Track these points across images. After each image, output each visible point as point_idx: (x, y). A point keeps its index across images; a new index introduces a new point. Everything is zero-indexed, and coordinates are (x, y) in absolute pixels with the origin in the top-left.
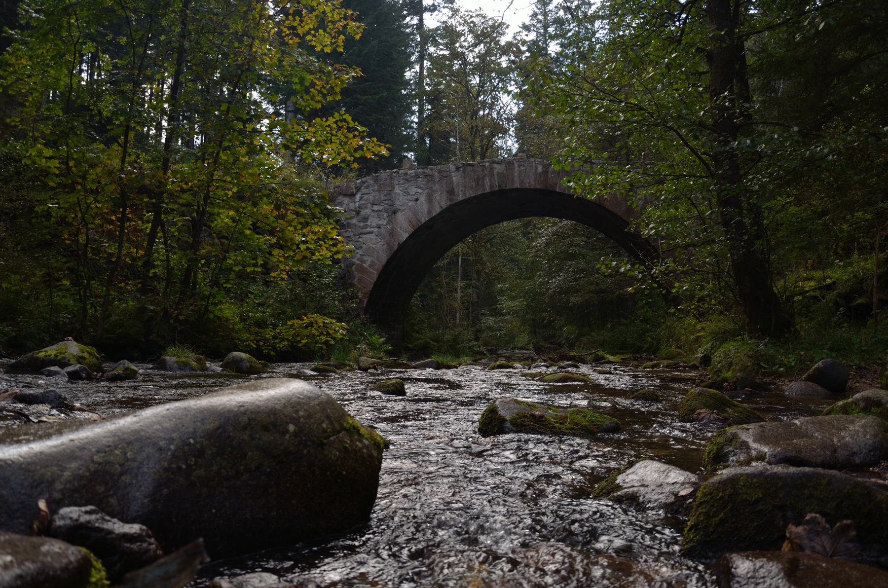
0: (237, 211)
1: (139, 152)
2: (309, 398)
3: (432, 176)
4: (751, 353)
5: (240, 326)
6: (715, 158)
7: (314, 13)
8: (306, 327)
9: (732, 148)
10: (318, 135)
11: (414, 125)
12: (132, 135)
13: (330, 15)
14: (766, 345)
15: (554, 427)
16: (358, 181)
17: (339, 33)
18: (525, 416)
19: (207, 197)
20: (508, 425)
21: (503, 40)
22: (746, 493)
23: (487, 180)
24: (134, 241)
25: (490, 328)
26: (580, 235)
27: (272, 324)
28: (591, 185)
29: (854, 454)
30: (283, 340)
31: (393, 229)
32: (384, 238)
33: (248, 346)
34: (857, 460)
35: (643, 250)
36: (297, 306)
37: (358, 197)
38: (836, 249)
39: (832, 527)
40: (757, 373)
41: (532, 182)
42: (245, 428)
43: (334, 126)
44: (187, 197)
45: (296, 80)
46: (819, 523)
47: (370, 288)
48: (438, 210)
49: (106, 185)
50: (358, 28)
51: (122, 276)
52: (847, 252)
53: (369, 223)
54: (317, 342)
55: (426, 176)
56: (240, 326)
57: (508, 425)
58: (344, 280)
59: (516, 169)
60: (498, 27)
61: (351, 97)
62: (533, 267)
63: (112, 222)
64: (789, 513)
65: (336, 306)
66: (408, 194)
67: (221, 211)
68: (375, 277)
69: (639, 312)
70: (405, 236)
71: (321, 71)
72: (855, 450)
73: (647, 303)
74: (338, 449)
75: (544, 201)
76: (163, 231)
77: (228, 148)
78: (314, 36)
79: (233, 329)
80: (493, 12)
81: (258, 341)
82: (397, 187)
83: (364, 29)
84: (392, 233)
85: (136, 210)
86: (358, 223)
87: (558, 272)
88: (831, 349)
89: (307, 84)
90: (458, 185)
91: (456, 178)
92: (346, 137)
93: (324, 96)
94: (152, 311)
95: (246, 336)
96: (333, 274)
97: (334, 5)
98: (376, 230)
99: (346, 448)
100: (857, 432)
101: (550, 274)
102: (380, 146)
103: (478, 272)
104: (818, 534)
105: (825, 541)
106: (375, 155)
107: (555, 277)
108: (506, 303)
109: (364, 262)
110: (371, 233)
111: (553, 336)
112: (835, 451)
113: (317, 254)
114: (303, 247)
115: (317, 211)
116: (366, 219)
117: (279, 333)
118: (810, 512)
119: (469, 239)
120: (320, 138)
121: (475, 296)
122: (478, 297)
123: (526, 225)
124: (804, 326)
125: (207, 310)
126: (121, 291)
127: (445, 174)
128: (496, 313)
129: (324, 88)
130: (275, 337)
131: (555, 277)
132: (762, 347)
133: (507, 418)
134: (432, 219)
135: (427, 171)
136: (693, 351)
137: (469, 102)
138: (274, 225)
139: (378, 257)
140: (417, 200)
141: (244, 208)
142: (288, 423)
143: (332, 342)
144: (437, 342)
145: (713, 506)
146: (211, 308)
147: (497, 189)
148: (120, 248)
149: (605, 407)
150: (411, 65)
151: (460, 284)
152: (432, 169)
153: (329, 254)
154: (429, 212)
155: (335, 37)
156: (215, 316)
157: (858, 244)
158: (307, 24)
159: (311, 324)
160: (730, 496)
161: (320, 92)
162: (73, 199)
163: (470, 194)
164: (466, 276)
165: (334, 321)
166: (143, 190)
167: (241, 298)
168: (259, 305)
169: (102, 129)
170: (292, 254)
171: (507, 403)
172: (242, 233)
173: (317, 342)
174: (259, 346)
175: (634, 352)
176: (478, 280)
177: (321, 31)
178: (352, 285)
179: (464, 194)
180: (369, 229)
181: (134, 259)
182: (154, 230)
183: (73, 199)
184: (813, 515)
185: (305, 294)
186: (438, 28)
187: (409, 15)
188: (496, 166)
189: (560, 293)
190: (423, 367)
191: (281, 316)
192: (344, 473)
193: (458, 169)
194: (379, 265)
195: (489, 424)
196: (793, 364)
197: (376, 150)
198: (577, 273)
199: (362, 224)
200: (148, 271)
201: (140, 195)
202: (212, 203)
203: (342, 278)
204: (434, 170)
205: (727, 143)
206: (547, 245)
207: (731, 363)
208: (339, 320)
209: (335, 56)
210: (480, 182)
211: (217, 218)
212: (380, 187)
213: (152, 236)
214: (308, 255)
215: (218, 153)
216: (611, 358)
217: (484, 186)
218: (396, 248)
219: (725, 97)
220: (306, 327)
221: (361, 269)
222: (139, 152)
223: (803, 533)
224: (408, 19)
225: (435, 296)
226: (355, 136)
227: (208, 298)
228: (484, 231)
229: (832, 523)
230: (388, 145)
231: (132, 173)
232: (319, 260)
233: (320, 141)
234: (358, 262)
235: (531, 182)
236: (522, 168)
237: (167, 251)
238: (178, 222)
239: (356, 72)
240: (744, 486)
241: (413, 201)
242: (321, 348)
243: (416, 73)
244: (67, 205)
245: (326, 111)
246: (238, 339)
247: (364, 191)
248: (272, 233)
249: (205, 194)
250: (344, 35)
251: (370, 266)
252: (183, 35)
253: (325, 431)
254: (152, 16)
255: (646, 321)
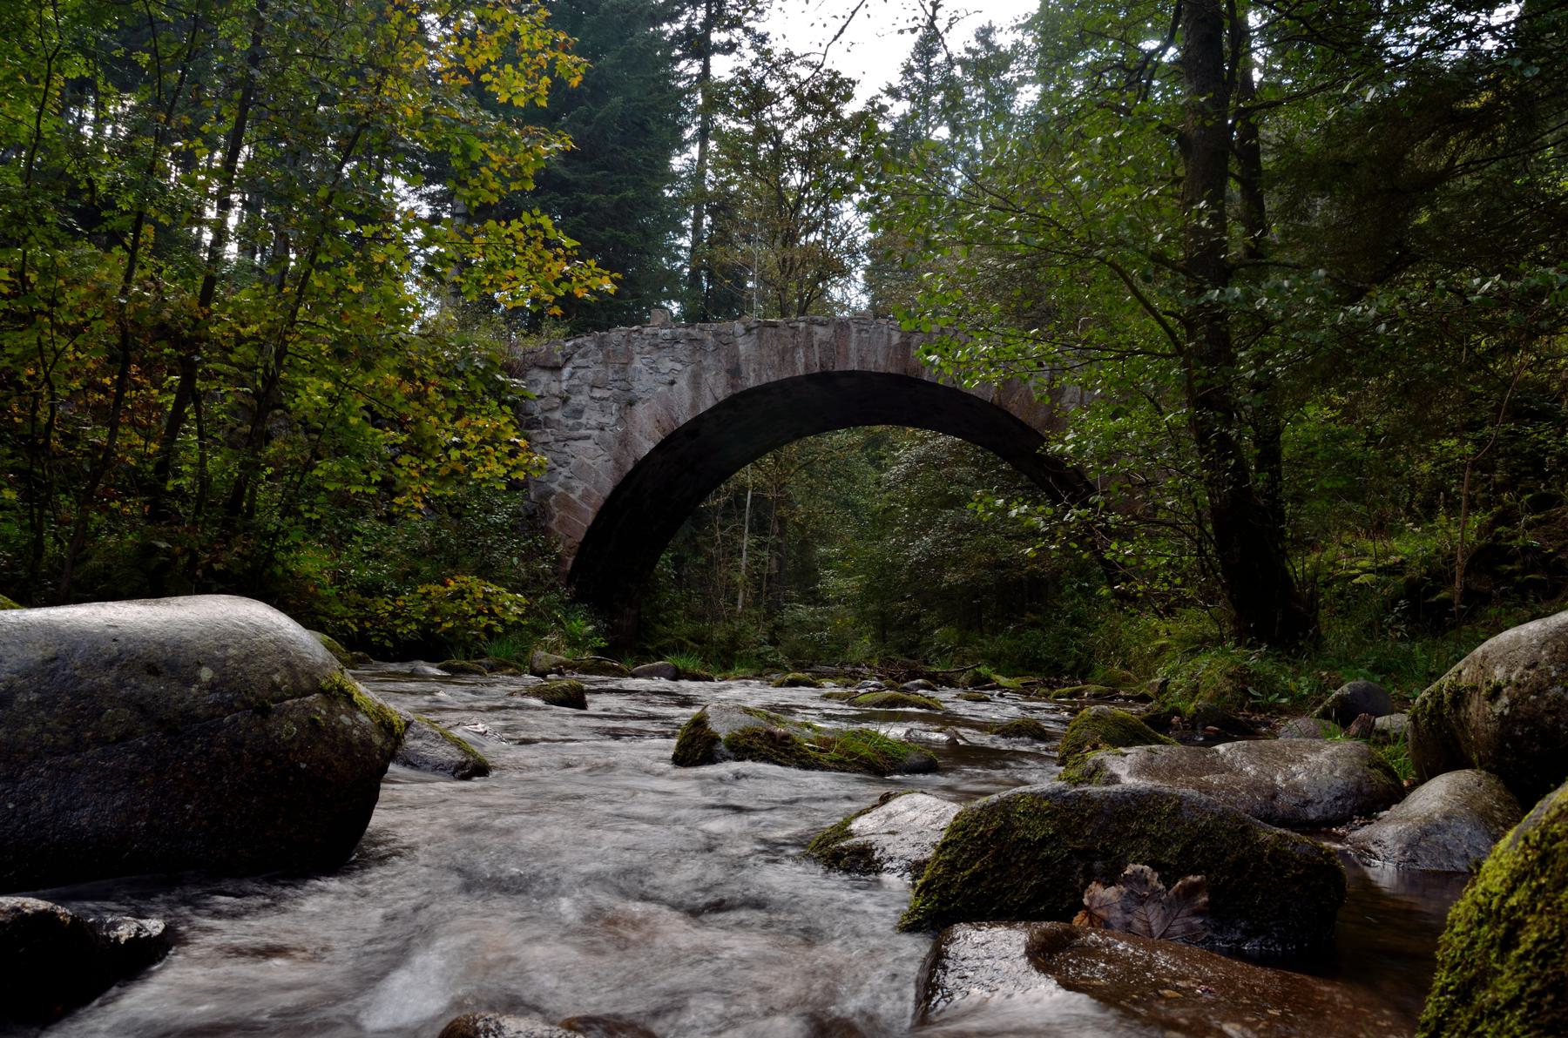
0: (337, 381)
1: (162, 264)
2: (258, 628)
3: (702, 341)
4: (1231, 670)
5: (332, 591)
6: (1187, 323)
7: (497, 34)
8: (452, 599)
9: (1209, 301)
10: (490, 251)
11: (682, 253)
12: (148, 231)
13: (525, 39)
14: (1263, 658)
15: (807, 757)
16: (570, 344)
17: (541, 72)
18: (756, 735)
19: (281, 353)
20: (722, 747)
21: (848, 110)
22: (1027, 827)
23: (800, 353)
24: (141, 426)
25: (801, 625)
26: (967, 464)
27: (393, 592)
28: (973, 362)
29: (1308, 803)
30: (409, 620)
31: (626, 433)
32: (610, 448)
33: (345, 628)
34: (1312, 813)
35: (1059, 482)
36: (442, 558)
37: (566, 372)
38: (1410, 503)
39: (1168, 888)
40: (1241, 706)
41: (881, 362)
42: (110, 664)
43: (521, 236)
44: (246, 351)
45: (456, 150)
46: (1147, 881)
47: (581, 537)
48: (710, 404)
49: (94, 319)
50: (576, 66)
51: (119, 488)
52: (1430, 510)
53: (583, 420)
54: (470, 627)
55: (692, 340)
56: (332, 591)
57: (722, 747)
58: (534, 520)
59: (854, 335)
60: (840, 87)
61: (551, 186)
62: (884, 520)
63: (103, 389)
64: (1098, 865)
65: (512, 566)
66: (657, 371)
67: (307, 380)
68: (590, 518)
69: (1066, 605)
70: (646, 447)
71: (500, 136)
72: (1310, 795)
73: (1080, 589)
74: (296, 723)
75: (897, 398)
76: (198, 410)
77: (327, 266)
78: (496, 75)
79: (318, 598)
80: (842, 63)
81: (362, 620)
82: (637, 358)
83: (587, 69)
84: (624, 441)
85: (149, 368)
86: (563, 420)
87: (924, 529)
88: (1375, 669)
89: (476, 158)
90: (747, 360)
91: (745, 347)
92: (540, 257)
93: (505, 182)
94: (166, 552)
95: (339, 609)
96: (510, 507)
97: (533, 21)
98: (596, 432)
99: (315, 721)
100: (1320, 767)
101: (912, 532)
102: (601, 275)
103: (782, 521)
104: (1141, 901)
105: (1153, 915)
106: (591, 291)
107: (919, 537)
108: (833, 582)
109: (572, 490)
110: (587, 438)
111: (914, 645)
112: (1274, 797)
113: (480, 469)
114: (455, 454)
115: (479, 388)
116: (578, 413)
117: (403, 608)
118: (1135, 862)
119: (768, 459)
120: (494, 258)
121: (774, 563)
122: (781, 566)
123: (875, 442)
124: (1338, 633)
125: (270, 557)
126: (115, 516)
127: (724, 339)
128: (815, 599)
129: (504, 166)
130: (394, 615)
131: (919, 537)
132: (1253, 660)
133: (722, 736)
134: (698, 421)
135: (694, 332)
136: (1150, 674)
137: (783, 218)
138: (403, 410)
139: (596, 482)
140: (672, 383)
141: (348, 378)
142: (200, 665)
143: (499, 629)
144: (700, 642)
145: (964, 850)
146: (281, 555)
147: (817, 370)
148: (112, 436)
149: (937, 741)
150: (682, 146)
151: (746, 541)
152: (702, 329)
153: (503, 471)
154: (694, 406)
155: (533, 80)
156: (287, 571)
157: (1446, 496)
158: (483, 52)
159: (460, 594)
160: (997, 832)
161: (498, 174)
162: (29, 339)
163: (770, 376)
164: (760, 527)
165: (503, 590)
166: (164, 331)
167: (339, 542)
168: (370, 555)
169: (91, 216)
170: (434, 465)
171: (727, 710)
172: (344, 422)
173: (470, 627)
174: (363, 630)
175: (1042, 671)
176: (781, 535)
177: (509, 68)
178: (546, 531)
179: (759, 376)
180: (583, 432)
181: (141, 458)
182: (179, 406)
183: (29, 339)
184: (1139, 867)
185: (460, 538)
186: (732, 82)
187: (684, 57)
188: (817, 329)
189: (928, 565)
190: (649, 674)
191: (409, 577)
192: (303, 766)
193: (748, 330)
194: (599, 498)
195: (690, 745)
196: (1305, 692)
197: (594, 283)
198: (959, 530)
199: (571, 422)
200: (165, 480)
201: (160, 345)
202: (290, 364)
203: (529, 517)
204: (705, 333)
205: (1201, 291)
206: (909, 477)
207: (1197, 686)
208: (513, 590)
209: (532, 115)
210: (788, 357)
211: (300, 392)
212: (607, 356)
213: (177, 418)
214: (462, 468)
215: (307, 274)
216: (1003, 680)
217: (793, 363)
218: (630, 467)
219: (1201, 211)
220: (452, 599)
221: (566, 503)
222: (162, 264)
223: (1115, 899)
224: (683, 64)
225: (701, 560)
226: (556, 257)
227: (275, 535)
228: (795, 447)
229: (1168, 881)
230: (615, 275)
231: (140, 298)
232: (484, 480)
233: (493, 263)
234: (560, 490)
235: (879, 362)
236: (864, 335)
237: (201, 446)
238: (224, 399)
239: (563, 142)
240: (1024, 814)
241: (663, 382)
242: (477, 638)
243: (692, 161)
244: (17, 352)
245: (508, 210)
246: (325, 614)
247: (578, 361)
248: (400, 424)
249: (277, 344)
250: (551, 76)
251: (582, 498)
252: (254, 59)
253: (275, 687)
254: (199, 24)
255: (1075, 621)
